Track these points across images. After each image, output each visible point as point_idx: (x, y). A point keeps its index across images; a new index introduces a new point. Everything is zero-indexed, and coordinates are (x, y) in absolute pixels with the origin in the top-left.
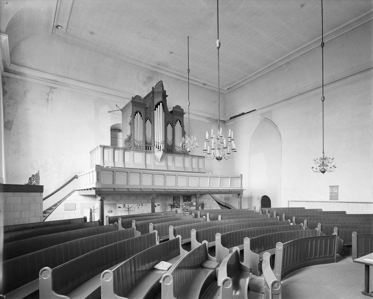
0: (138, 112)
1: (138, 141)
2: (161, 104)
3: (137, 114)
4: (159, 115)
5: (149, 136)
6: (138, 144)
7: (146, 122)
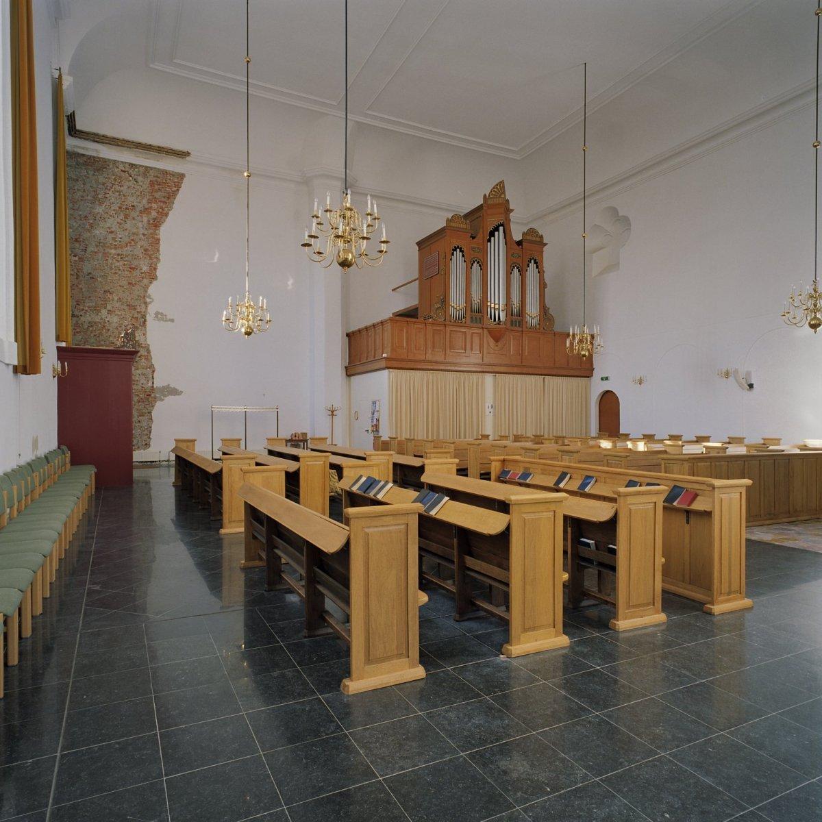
3: (455, 252)
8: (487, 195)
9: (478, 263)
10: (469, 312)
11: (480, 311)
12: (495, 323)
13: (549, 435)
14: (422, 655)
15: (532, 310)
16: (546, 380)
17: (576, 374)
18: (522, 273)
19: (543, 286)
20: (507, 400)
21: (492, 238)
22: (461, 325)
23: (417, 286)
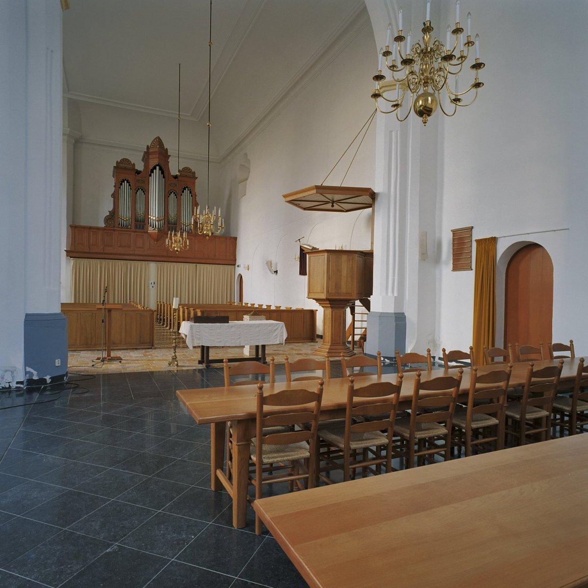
0: (125, 180)
1: (125, 217)
2: (157, 167)
3: (123, 183)
4: (155, 183)
5: (172, 213)
6: (125, 222)
7: (136, 193)
8: (149, 145)
9: (174, 193)
10: (134, 221)
11: (175, 224)
13: (118, 302)
16: (198, 267)
17: (77, 256)
20: (120, 275)
22: (128, 230)
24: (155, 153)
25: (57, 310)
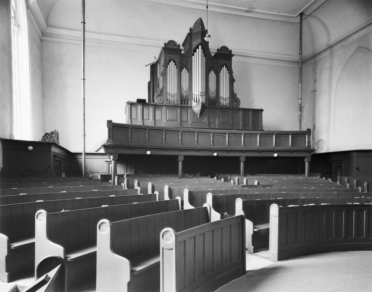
2: (200, 47)
3: (170, 63)
4: (198, 60)
6: (172, 98)
12: (197, 103)
14: (267, 247)
15: (224, 93)
18: (217, 74)
19: (232, 81)
21: (195, 53)
23: (168, 200)
24: (197, 33)
25: (7, 274)
